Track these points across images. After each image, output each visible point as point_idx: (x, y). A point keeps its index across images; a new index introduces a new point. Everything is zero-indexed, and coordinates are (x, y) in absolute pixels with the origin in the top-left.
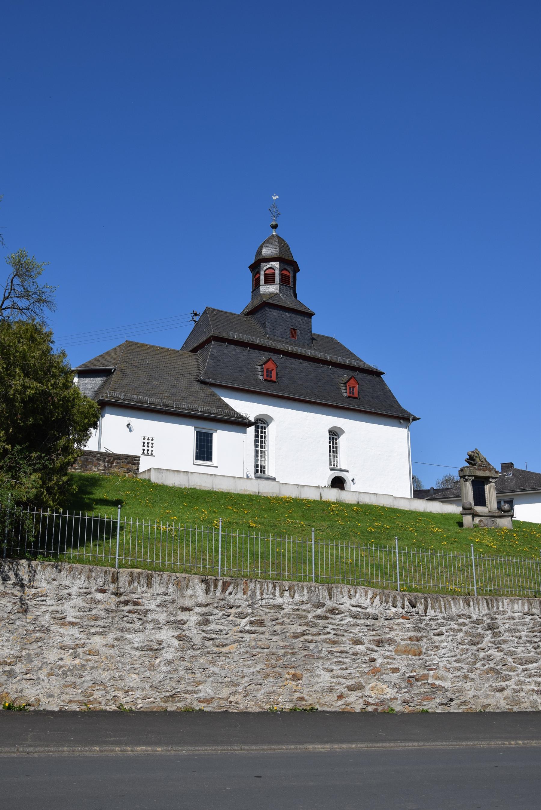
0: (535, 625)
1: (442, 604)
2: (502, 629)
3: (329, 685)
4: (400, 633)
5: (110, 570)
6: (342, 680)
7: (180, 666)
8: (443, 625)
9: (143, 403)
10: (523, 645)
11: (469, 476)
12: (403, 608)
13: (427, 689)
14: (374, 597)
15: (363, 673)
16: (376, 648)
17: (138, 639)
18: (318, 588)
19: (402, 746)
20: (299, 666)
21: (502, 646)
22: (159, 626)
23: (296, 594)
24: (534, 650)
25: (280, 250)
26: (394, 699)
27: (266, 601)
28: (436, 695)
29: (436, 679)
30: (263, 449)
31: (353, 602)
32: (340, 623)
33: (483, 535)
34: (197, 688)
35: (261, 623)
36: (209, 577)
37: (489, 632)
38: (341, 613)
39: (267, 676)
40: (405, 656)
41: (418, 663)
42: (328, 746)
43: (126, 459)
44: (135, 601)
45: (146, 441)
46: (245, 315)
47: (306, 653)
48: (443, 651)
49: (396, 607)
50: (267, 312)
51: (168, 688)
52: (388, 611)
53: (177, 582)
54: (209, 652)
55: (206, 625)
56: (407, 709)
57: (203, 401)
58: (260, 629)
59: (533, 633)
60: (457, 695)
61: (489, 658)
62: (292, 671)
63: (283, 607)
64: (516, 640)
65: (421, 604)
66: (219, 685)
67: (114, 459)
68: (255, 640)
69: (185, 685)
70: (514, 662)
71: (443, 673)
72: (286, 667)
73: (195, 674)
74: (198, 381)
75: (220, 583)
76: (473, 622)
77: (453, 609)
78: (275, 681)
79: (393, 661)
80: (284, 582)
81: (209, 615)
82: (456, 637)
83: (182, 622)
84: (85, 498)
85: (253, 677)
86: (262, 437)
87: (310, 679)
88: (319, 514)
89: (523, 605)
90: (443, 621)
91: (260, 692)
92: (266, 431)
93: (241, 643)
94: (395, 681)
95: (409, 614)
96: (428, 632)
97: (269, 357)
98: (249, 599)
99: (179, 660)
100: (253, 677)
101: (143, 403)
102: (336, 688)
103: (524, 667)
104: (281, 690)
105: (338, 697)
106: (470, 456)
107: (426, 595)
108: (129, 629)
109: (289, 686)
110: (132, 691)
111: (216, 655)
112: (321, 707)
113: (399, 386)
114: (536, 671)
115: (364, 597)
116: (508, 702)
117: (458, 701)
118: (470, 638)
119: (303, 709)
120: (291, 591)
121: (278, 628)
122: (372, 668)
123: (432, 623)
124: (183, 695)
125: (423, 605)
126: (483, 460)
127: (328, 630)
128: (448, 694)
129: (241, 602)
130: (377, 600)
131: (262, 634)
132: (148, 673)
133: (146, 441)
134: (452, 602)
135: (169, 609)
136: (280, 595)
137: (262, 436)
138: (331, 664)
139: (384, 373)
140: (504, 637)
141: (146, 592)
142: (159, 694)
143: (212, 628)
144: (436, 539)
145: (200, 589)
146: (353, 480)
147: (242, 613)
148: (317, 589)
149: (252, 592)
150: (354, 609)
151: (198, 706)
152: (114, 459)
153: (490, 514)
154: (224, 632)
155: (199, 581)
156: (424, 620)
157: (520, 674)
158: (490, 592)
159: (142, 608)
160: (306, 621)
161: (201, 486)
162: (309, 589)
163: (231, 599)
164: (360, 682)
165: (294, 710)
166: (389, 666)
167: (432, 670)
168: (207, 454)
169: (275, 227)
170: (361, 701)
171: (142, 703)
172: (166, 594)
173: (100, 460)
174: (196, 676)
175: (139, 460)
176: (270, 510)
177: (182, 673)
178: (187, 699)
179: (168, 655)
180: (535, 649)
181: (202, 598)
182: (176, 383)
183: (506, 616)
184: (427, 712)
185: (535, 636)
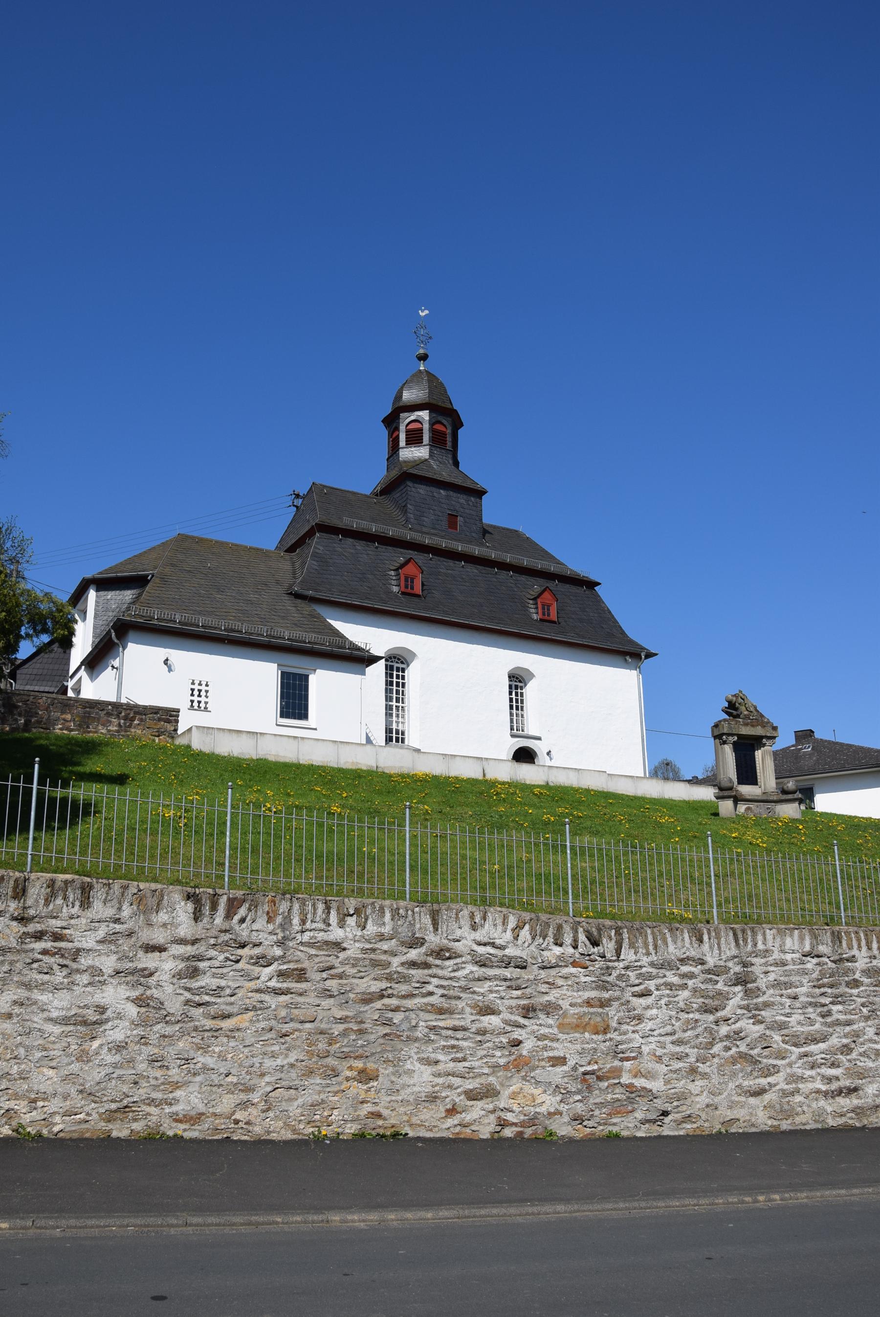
0: (823, 975)
1: (650, 939)
2: (762, 982)
3: (429, 1089)
4: (569, 993)
5: (11, 874)
6: (456, 1081)
7: (140, 1055)
8: (650, 977)
9: (192, 625)
10: (800, 1011)
11: (728, 735)
12: (575, 947)
13: (619, 1094)
14: (519, 927)
15: (495, 1067)
16: (522, 1021)
17: (59, 1003)
18: (413, 911)
19: (533, 1214)
20: (373, 1054)
21: (763, 1013)
22: (101, 979)
23: (370, 922)
24: (821, 1019)
25: (430, 392)
26: (555, 1114)
27: (312, 934)
28: (636, 1106)
29: (635, 1076)
30: (400, 704)
31: (479, 935)
32: (452, 975)
33: (747, 827)
34: (171, 1096)
35: (301, 975)
36: (201, 890)
37: (739, 988)
38: (456, 957)
39: (310, 1073)
40: (577, 1035)
41: (603, 1046)
42: (373, 1216)
43: (155, 713)
44: (57, 933)
45: (196, 687)
46: (377, 495)
47: (387, 1030)
48: (650, 1025)
49: (561, 945)
50: (409, 489)
51: (115, 1094)
52: (545, 953)
53: (140, 899)
54: (196, 1029)
55: (191, 978)
56: (579, 1132)
57: (295, 624)
58: (299, 985)
59: (819, 988)
60: (675, 1104)
61: (738, 1036)
62: (359, 1064)
63: (345, 945)
64: (788, 1002)
65: (610, 938)
66: (214, 1089)
67: (136, 713)
68: (287, 1006)
69: (148, 1090)
70: (783, 1042)
71: (648, 1064)
72: (346, 1057)
73: (168, 1068)
74: (291, 594)
75: (223, 901)
76: (709, 972)
77: (671, 948)
78: (324, 1082)
79: (555, 1045)
80: (346, 900)
81: (200, 961)
82: (676, 999)
83: (146, 972)
84: (62, 771)
85: (282, 1075)
86: (398, 684)
87: (393, 1078)
88: (472, 798)
89: (802, 939)
90: (651, 970)
91: (296, 1104)
92: (406, 674)
93: (259, 1012)
94: (558, 1080)
95: (587, 958)
96: (622, 990)
97: (409, 557)
98: (278, 931)
99: (138, 1042)
100: (282, 1075)
101: (192, 625)
102: (443, 1094)
103: (802, 1050)
104: (336, 1098)
105: (448, 1111)
106: (730, 702)
107: (619, 923)
108: (43, 984)
109: (352, 1092)
110: (44, 1100)
111: (210, 1034)
112: (414, 1130)
113: (625, 605)
114: (823, 1056)
115: (500, 928)
116: (773, 1113)
117: (676, 1115)
118: (702, 1000)
119: (378, 1135)
120: (359, 916)
121: (333, 984)
122: (514, 1057)
123: (630, 974)
124: (144, 1107)
125: (613, 941)
126: (752, 709)
127: (430, 988)
128: (659, 1104)
129: (262, 936)
130: (525, 933)
131: (301, 995)
132: (75, 1067)
133: (196, 687)
134: (668, 935)
135: (121, 948)
136: (338, 924)
137: (398, 683)
138: (434, 1051)
139: (599, 584)
140: (765, 996)
141: (78, 917)
142: (97, 1105)
143: (203, 984)
144: (662, 834)
145: (183, 910)
146: (549, 753)
147: (264, 957)
148: (410, 912)
149: (285, 918)
150: (481, 950)
151: (171, 1129)
152: (135, 713)
153: (765, 798)
154: (228, 991)
155: (180, 897)
156: (614, 968)
157: (795, 1063)
158: (746, 919)
159: (70, 945)
160: (387, 971)
161: (278, 756)
162: (395, 913)
163: (243, 930)
164: (490, 1085)
165: (360, 1136)
166: (546, 1054)
167: (628, 1059)
168: (300, 709)
169: (423, 358)
170: (492, 1117)
171: (63, 1122)
172: (117, 921)
173: (112, 715)
174: (170, 1073)
175: (178, 716)
176: (389, 792)
177: (142, 1067)
178: (150, 1115)
179: (117, 1033)
180: (823, 1016)
181: (185, 927)
182: (253, 597)
183: (770, 958)
184: (617, 1136)
185: (823, 994)
